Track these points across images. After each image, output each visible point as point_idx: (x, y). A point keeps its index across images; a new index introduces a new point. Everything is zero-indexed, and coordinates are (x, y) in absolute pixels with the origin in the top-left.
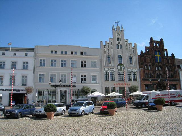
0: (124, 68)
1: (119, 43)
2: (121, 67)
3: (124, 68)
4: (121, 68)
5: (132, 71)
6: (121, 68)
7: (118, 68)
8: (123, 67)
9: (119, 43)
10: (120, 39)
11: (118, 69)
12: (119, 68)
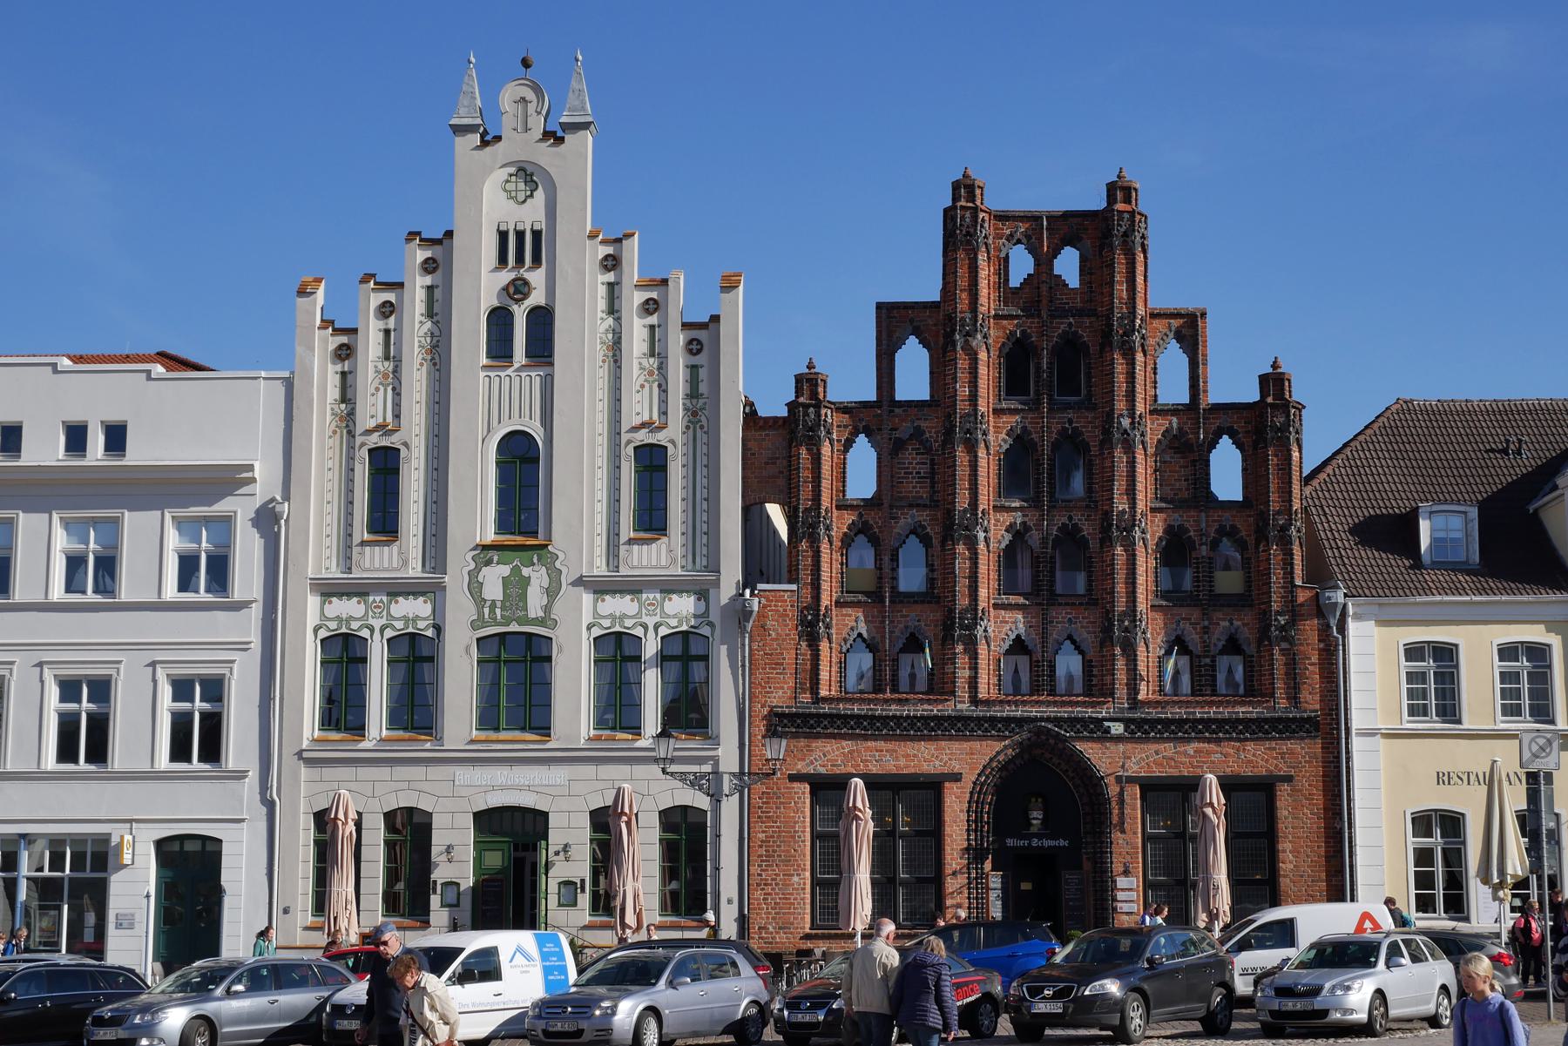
0: (552, 592)
2: (516, 571)
3: (552, 592)
4: (516, 587)
5: (651, 622)
6: (516, 587)
7: (475, 588)
8: (537, 577)
11: (480, 601)
12: (493, 589)
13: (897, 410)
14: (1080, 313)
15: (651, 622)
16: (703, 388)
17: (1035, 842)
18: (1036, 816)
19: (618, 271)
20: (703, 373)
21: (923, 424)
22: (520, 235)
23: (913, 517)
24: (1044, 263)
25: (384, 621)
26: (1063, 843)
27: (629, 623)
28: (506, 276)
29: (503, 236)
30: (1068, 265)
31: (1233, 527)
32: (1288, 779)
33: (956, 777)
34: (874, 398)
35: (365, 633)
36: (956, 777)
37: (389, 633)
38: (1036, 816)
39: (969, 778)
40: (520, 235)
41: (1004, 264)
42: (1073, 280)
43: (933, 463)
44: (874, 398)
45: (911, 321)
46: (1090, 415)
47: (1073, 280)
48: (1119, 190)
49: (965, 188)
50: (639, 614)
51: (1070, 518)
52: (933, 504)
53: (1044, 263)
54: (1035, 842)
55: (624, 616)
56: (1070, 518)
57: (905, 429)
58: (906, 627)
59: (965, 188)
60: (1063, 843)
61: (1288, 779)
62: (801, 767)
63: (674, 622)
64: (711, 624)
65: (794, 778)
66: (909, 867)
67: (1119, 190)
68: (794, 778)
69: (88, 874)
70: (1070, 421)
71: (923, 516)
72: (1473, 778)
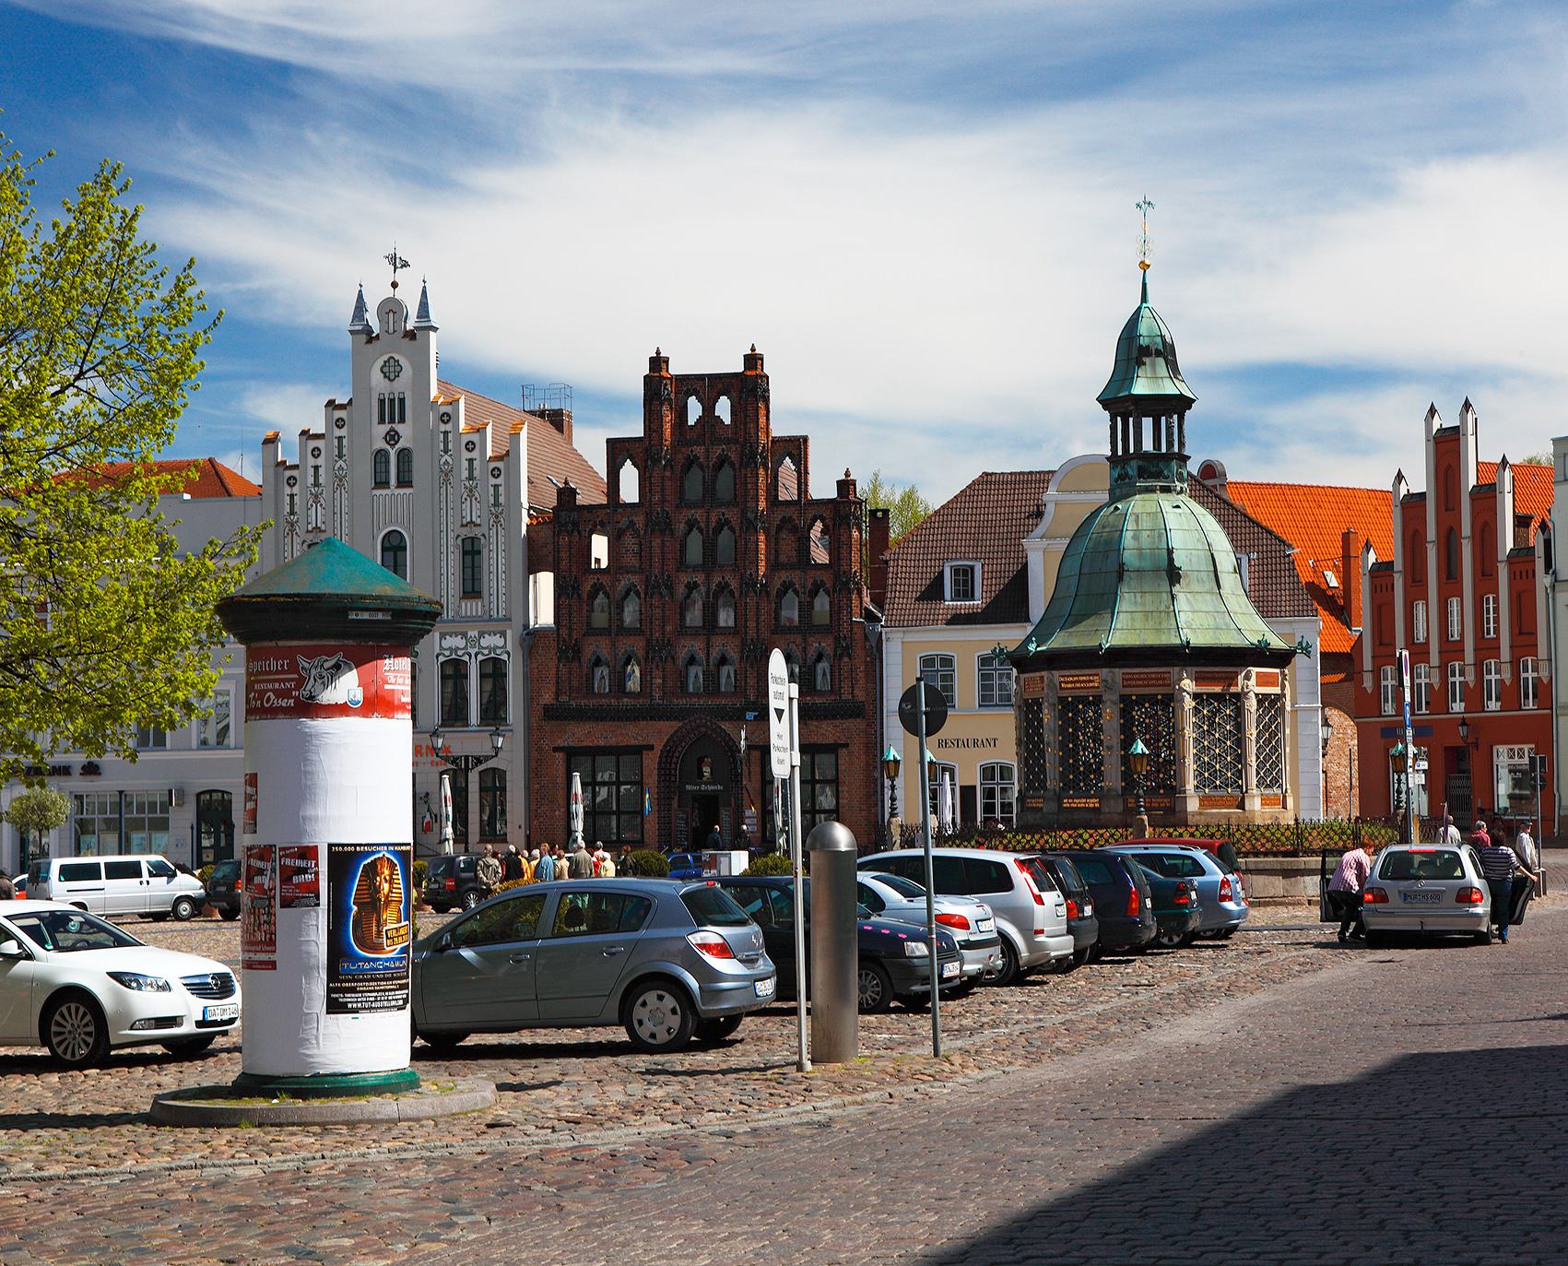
1: (392, 437)
5: (473, 652)
9: (392, 437)
10: (402, 401)
13: (620, 510)
14: (728, 442)
15: (473, 652)
16: (502, 500)
17: (703, 787)
18: (707, 770)
19: (573, 409)
20: (501, 489)
21: (635, 519)
22: (392, 401)
23: (629, 579)
24: (709, 408)
25: (476, 650)
26: (720, 787)
27: (460, 653)
28: (386, 427)
29: (382, 402)
30: (723, 408)
31: (822, 581)
32: (846, 745)
33: (651, 748)
34: (637, 500)
35: (466, 658)
36: (651, 748)
37: (480, 657)
38: (707, 770)
39: (658, 748)
40: (392, 401)
41: (682, 412)
42: (727, 420)
43: (641, 544)
44: (637, 500)
45: (628, 450)
46: (735, 510)
47: (727, 420)
48: (753, 360)
49: (658, 362)
50: (466, 648)
51: (723, 578)
52: (641, 571)
53: (709, 408)
54: (703, 787)
55: (496, 647)
56: (723, 578)
57: (624, 522)
58: (626, 651)
59: (658, 362)
60: (720, 787)
61: (846, 745)
62: (560, 743)
63: (447, 653)
64: (508, 653)
65: (556, 749)
66: (1143, 820)
67: (753, 360)
68: (556, 749)
69: (158, 815)
70: (723, 514)
71: (635, 579)
72: (960, 743)
